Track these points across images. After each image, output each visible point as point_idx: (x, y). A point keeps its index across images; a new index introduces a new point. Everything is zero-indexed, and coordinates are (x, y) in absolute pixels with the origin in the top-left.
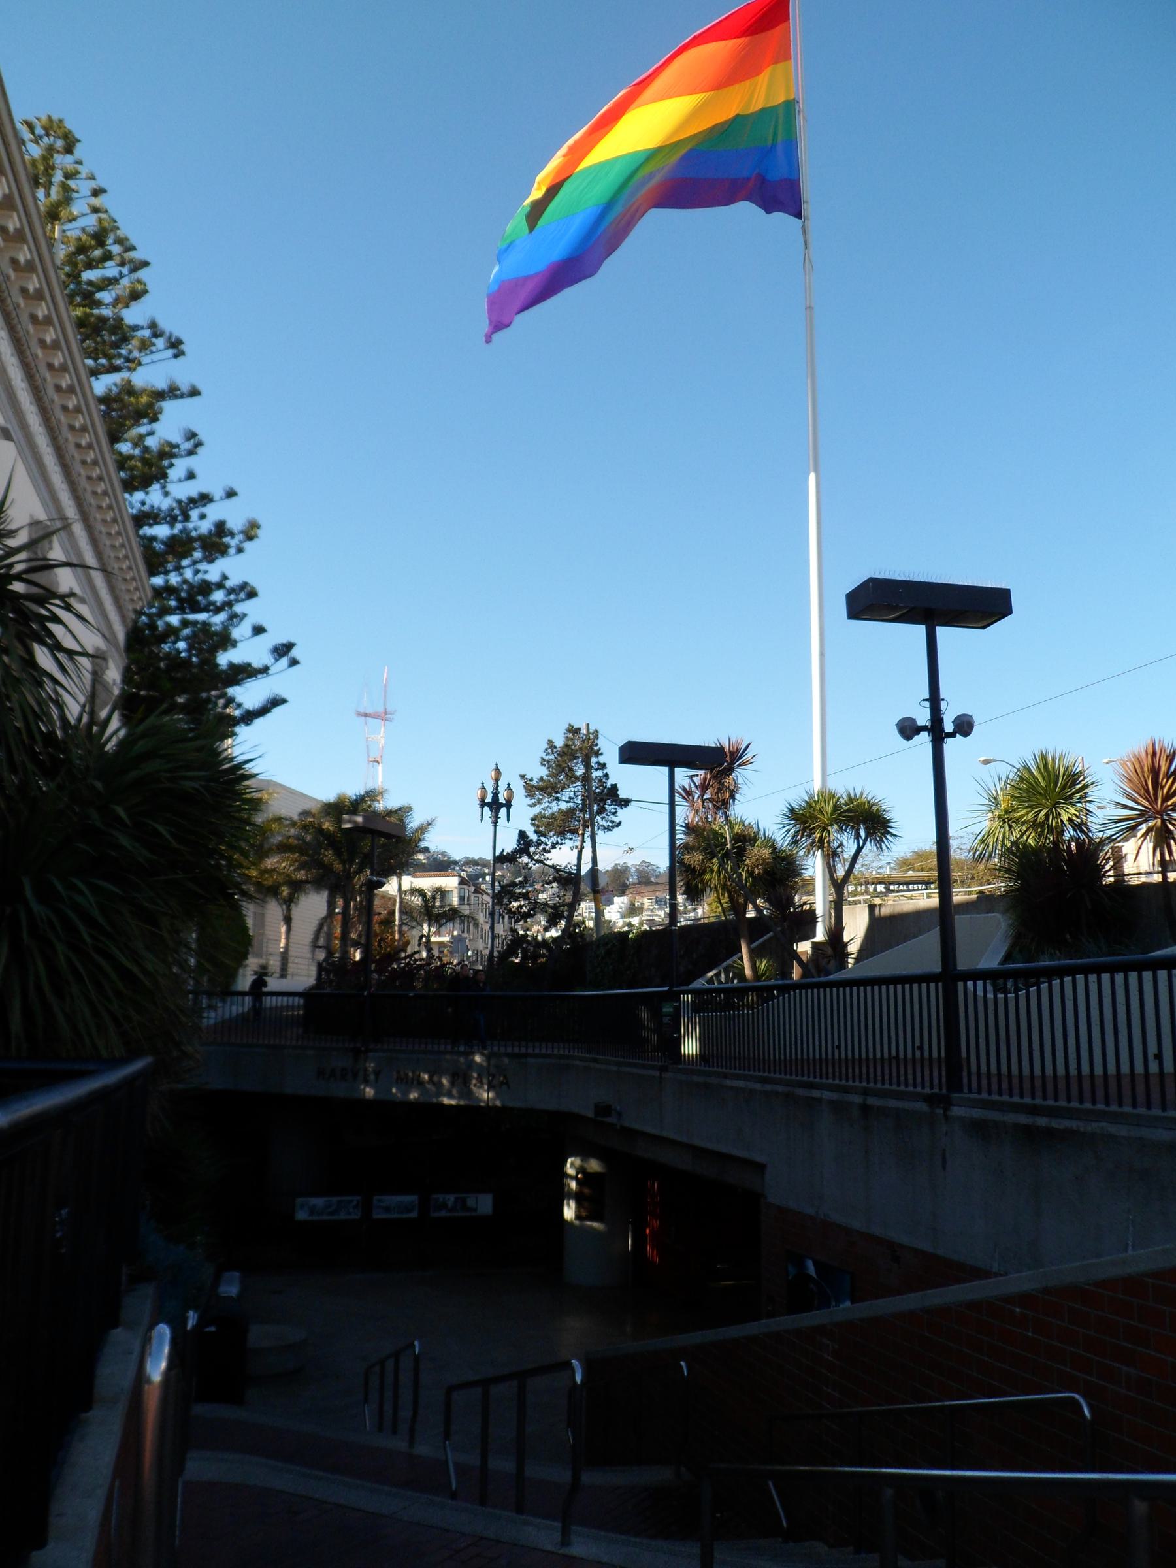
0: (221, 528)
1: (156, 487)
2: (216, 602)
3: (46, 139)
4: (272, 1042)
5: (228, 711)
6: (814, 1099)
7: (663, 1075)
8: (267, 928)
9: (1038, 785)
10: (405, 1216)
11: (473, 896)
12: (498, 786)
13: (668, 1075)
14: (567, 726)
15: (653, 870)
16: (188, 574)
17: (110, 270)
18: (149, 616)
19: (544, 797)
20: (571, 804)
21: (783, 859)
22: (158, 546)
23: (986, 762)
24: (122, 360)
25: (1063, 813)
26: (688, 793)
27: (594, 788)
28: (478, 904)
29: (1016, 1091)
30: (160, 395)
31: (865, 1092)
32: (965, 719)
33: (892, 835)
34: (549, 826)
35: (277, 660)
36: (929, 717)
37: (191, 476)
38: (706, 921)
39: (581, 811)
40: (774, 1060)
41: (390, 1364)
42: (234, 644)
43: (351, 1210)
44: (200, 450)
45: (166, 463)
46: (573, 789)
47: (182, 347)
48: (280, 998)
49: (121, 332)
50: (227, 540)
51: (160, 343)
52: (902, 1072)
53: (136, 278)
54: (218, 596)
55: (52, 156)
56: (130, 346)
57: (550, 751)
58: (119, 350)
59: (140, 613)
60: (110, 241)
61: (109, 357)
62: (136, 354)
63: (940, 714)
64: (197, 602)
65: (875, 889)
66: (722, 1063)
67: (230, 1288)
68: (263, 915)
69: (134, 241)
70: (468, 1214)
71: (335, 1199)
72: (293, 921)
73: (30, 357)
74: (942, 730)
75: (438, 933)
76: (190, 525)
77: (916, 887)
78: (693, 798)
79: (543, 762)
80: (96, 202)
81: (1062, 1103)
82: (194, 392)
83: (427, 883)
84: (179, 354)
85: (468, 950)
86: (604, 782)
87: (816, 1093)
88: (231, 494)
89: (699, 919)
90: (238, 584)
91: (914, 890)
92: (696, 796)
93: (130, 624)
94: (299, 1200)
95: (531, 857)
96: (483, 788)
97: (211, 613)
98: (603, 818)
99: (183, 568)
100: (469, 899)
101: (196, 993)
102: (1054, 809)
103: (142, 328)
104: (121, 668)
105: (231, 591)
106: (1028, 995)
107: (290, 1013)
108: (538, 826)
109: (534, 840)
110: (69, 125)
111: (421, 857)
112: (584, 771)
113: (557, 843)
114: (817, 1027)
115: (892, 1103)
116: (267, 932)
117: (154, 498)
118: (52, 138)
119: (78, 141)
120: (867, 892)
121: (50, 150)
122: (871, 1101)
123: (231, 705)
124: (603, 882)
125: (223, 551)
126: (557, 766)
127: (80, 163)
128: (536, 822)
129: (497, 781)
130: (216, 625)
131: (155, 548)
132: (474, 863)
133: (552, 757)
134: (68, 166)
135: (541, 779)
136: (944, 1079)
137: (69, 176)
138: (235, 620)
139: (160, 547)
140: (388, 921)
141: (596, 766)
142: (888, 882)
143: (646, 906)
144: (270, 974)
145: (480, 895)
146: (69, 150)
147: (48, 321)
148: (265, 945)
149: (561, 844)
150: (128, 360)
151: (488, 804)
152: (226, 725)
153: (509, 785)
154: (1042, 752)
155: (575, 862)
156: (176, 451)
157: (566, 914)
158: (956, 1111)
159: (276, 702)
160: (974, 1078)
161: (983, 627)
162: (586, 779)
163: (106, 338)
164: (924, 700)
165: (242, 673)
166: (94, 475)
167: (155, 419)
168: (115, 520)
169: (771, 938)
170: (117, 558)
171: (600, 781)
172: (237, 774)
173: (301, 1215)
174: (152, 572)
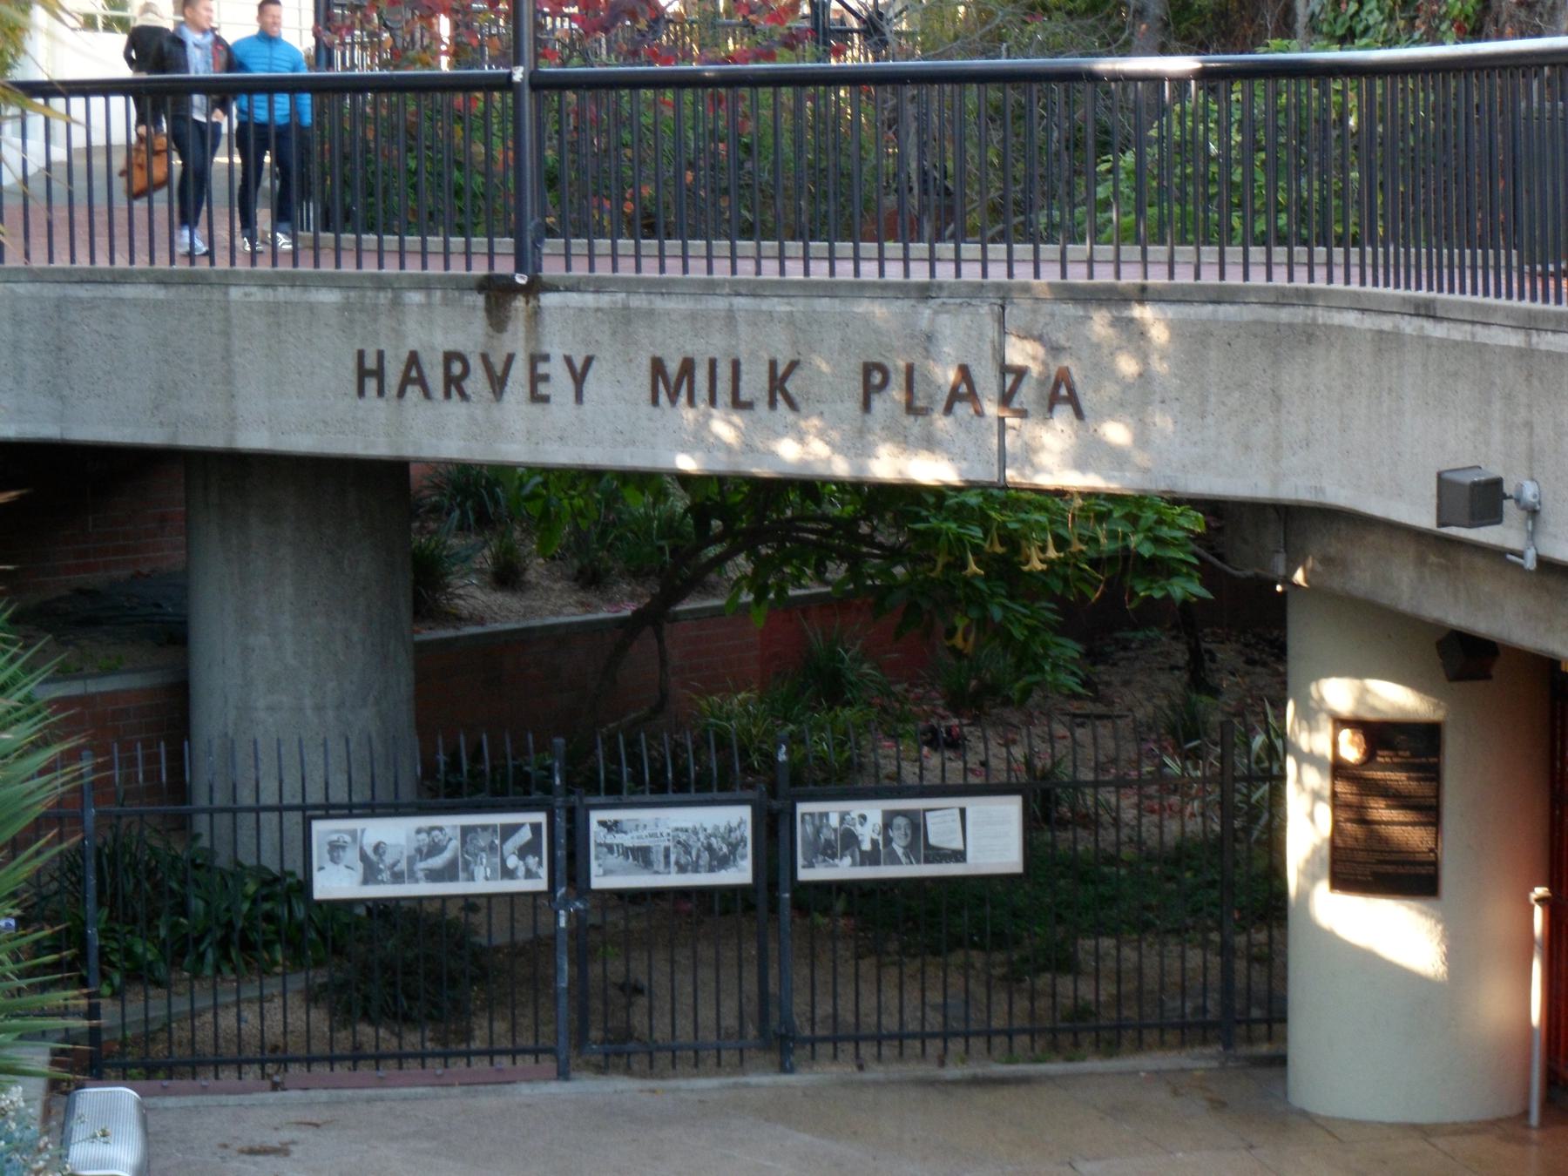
40: (1474, 268)
43: (512, 862)
71: (452, 823)
94: (322, 830)
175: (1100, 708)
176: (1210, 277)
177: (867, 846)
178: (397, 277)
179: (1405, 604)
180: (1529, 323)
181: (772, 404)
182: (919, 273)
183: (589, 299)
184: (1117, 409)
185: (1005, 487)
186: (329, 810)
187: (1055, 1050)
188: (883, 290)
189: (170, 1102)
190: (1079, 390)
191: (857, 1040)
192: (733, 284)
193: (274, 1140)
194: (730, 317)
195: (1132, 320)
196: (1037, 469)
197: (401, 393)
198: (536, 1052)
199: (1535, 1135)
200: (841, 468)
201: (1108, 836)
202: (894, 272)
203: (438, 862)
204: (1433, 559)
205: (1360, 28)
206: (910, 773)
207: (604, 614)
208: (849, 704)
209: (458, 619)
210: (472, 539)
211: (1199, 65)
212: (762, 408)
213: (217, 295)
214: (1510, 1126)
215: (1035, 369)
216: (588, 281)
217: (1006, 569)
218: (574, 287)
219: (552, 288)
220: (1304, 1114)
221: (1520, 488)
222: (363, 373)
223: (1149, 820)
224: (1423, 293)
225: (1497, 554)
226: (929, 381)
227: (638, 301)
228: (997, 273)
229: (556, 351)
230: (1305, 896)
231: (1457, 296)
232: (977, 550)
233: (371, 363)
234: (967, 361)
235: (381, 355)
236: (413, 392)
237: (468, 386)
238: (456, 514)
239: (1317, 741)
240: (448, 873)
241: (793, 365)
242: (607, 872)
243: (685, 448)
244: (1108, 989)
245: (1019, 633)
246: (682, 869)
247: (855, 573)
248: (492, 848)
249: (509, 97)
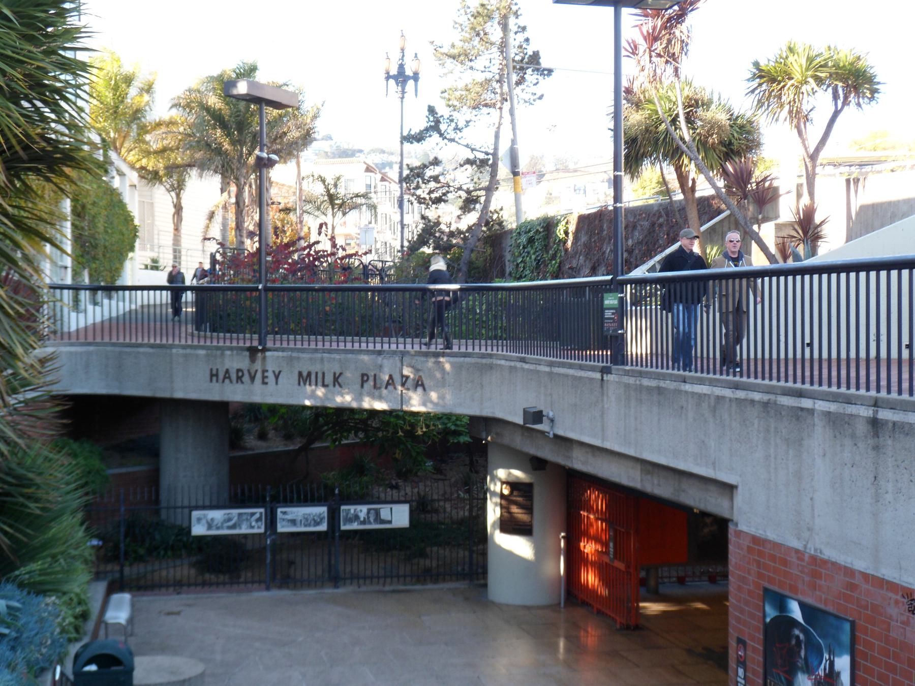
6: (802, 409)
7: (605, 378)
11: (380, 184)
31: (876, 404)
43: (254, 524)
57: (462, 11)
71: (235, 512)
86: (525, 49)
87: (806, 403)
94: (195, 514)
122: (884, 414)
141: (515, 29)
144: (161, 268)
148: (156, 237)
153: (416, 54)
157: (482, 199)
173: (198, 530)
175: (442, 477)
176: (463, 350)
178: (223, 347)
179: (518, 447)
180: (551, 364)
181: (334, 385)
182: (378, 347)
183: (280, 354)
184: (436, 388)
185: (402, 411)
186: (197, 508)
187: (418, 581)
188: (368, 352)
189: (144, 598)
190: (425, 382)
191: (358, 578)
192: (323, 349)
193: (176, 610)
194: (322, 359)
195: (440, 362)
196: (412, 406)
197: (223, 381)
198: (260, 582)
199: (562, 610)
200: (354, 405)
201: (442, 516)
202: (371, 346)
203: (231, 523)
204: (526, 434)
205: (524, 275)
206: (382, 496)
207: (291, 448)
208: (366, 475)
209: (246, 449)
210: (252, 425)
211: (773, 253)
212: (331, 387)
213: (168, 351)
214: (554, 607)
215: (412, 376)
216: (279, 348)
217: (411, 434)
218: (276, 350)
219: (269, 350)
220: (493, 603)
221: (548, 413)
222: (212, 375)
223: (454, 512)
224: (523, 355)
225: (542, 433)
226: (381, 380)
227: (295, 354)
228: (401, 347)
229: (270, 369)
230: (492, 535)
231: (532, 356)
232: (402, 428)
233: (214, 372)
234: (392, 373)
235: (217, 370)
236: (227, 381)
237: (244, 379)
238: (248, 417)
239: (496, 487)
240: (234, 527)
241: (341, 374)
242: (283, 527)
243: (308, 399)
244: (434, 564)
245: (414, 454)
246: (305, 526)
247: (367, 436)
248: (247, 519)
249: (258, 293)
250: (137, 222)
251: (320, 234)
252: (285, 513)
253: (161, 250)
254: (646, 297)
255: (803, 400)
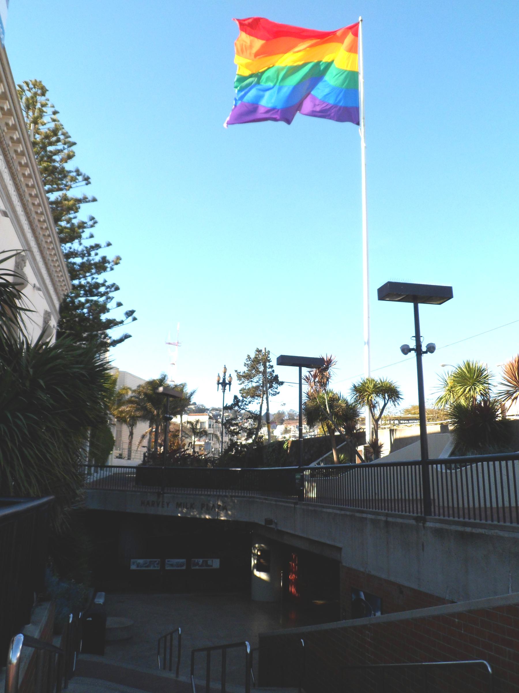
0: (104, 260)
1: (77, 241)
2: (101, 292)
3: (34, 90)
4: (121, 489)
5: (105, 340)
6: (363, 518)
7: (296, 506)
8: (122, 437)
9: (465, 375)
10: (179, 568)
11: (215, 424)
12: (225, 375)
13: (298, 506)
14: (256, 349)
15: (295, 413)
16: (89, 279)
17: (60, 146)
18: (71, 297)
19: (245, 381)
20: (258, 384)
21: (351, 409)
22: (77, 267)
23: (443, 366)
24: (63, 186)
25: (477, 388)
26: (307, 379)
27: (268, 376)
28: (217, 428)
29: (456, 515)
30: (79, 201)
31: (387, 515)
32: (431, 345)
33: (401, 398)
34: (248, 393)
35: (127, 318)
36: (415, 344)
37: (92, 236)
38: (318, 436)
39: (262, 387)
40: (341, 499)
41: (169, 637)
42: (108, 310)
43: (156, 565)
44: (96, 225)
45: (81, 230)
46: (258, 377)
47: (90, 180)
48: (128, 469)
49: (64, 173)
50: (107, 265)
51: (80, 178)
52: (407, 505)
53: (71, 150)
54: (102, 289)
55: (36, 97)
56: (67, 180)
57: (248, 360)
58: (62, 182)
59: (67, 296)
60: (60, 133)
61: (57, 184)
62: (69, 183)
63: (420, 343)
64: (93, 292)
65: (394, 423)
66: (328, 502)
67: (100, 600)
68: (121, 431)
69: (70, 134)
70: (208, 568)
71: (149, 560)
72: (134, 434)
73: (18, 181)
74: (421, 350)
75: (199, 440)
76: (91, 258)
77: (412, 421)
78: (311, 381)
79: (245, 365)
80: (54, 117)
81: (478, 521)
82: (94, 200)
83: (193, 418)
84: (88, 183)
85: (212, 448)
87: (364, 515)
88: (109, 244)
89: (316, 435)
90: (111, 284)
91: (411, 423)
92: (312, 380)
93: (62, 301)
94: (132, 560)
95: (239, 407)
96: (219, 376)
97: (99, 297)
98: (271, 390)
99: (87, 276)
100: (213, 425)
101: (90, 466)
102: (473, 386)
103: (73, 172)
104: (57, 320)
105: (108, 287)
106: (461, 471)
107: (132, 476)
108: (243, 394)
109: (241, 400)
110: (44, 83)
111: (192, 407)
112: (263, 369)
113: (251, 401)
114: (359, 484)
115: (399, 520)
116: (122, 439)
117: (75, 246)
118: (36, 89)
119: (48, 90)
120: (390, 423)
121: (36, 94)
122: (390, 519)
123: (107, 338)
124: (271, 419)
125: (105, 269)
126: (251, 366)
127: (48, 100)
128: (242, 392)
129: (225, 373)
130: (101, 301)
131: (75, 268)
132: (216, 410)
133: (249, 362)
134: (43, 101)
135: (244, 372)
136: (423, 510)
137: (43, 105)
138: (109, 300)
139: (77, 268)
140: (175, 436)
142: (399, 419)
143: (292, 430)
145: (218, 424)
146: (43, 94)
147: (26, 165)
148: (121, 445)
149: (253, 401)
150: (66, 186)
151: (221, 383)
152: (104, 346)
153: (230, 375)
154: (467, 360)
155: (259, 410)
156: (85, 225)
158: (429, 524)
159: (127, 337)
160: (437, 508)
161: (440, 304)
162: (264, 373)
163: (57, 176)
164: (413, 337)
165: (111, 323)
166: (46, 234)
167: (76, 211)
168: (55, 255)
169: (345, 445)
170: (56, 271)
171: (271, 373)
172: (104, 367)
173: (133, 567)
174: (73, 278)
176: (242, 495)
177: (200, 564)
184: (230, 510)
200: (198, 516)
203: (146, 565)
215: (222, 505)
250: (115, 439)
251: (189, 446)
252: (168, 561)
253: (123, 451)
254: (316, 474)
255: (363, 514)
